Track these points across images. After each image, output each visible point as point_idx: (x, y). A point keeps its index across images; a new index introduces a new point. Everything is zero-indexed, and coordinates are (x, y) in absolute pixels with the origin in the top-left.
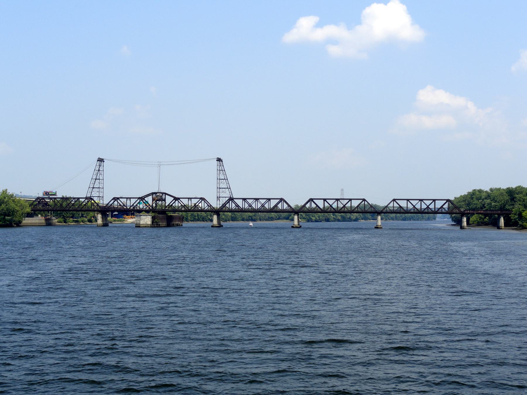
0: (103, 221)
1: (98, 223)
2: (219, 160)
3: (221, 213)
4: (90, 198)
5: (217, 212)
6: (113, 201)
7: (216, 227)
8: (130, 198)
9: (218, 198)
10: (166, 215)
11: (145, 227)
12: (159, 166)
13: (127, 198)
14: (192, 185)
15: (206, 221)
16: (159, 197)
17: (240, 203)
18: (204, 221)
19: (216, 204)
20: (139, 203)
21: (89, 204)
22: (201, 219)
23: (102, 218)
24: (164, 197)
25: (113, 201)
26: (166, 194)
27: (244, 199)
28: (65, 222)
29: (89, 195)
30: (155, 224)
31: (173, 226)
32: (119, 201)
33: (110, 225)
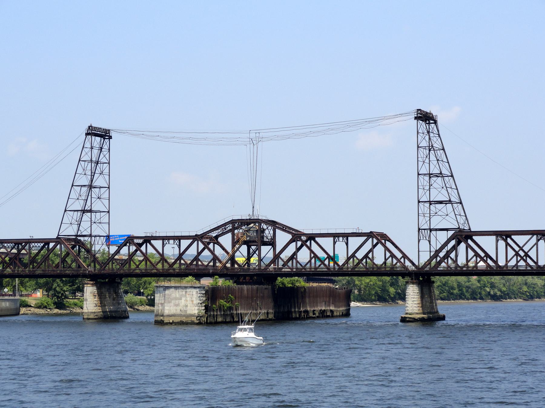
0: (102, 304)
1: (85, 310)
2: (425, 117)
3: (438, 280)
4: (76, 242)
5: (423, 277)
6: (453, 243)
7: (414, 320)
8: (346, 236)
9: (425, 232)
10: (273, 287)
11: (181, 323)
12: (255, 140)
13: (335, 236)
14: (346, 194)
15: (481, 298)
16: (252, 231)
17: (488, 243)
18: (475, 299)
19: (418, 253)
20: (454, 248)
21: (139, 257)
22: (468, 295)
23: (101, 296)
24: (268, 233)
25: (453, 243)
26: (274, 224)
27: (504, 235)
28: (60, 305)
29: (70, 231)
30: (218, 314)
31: (305, 317)
32: (314, 247)
33: (133, 317)
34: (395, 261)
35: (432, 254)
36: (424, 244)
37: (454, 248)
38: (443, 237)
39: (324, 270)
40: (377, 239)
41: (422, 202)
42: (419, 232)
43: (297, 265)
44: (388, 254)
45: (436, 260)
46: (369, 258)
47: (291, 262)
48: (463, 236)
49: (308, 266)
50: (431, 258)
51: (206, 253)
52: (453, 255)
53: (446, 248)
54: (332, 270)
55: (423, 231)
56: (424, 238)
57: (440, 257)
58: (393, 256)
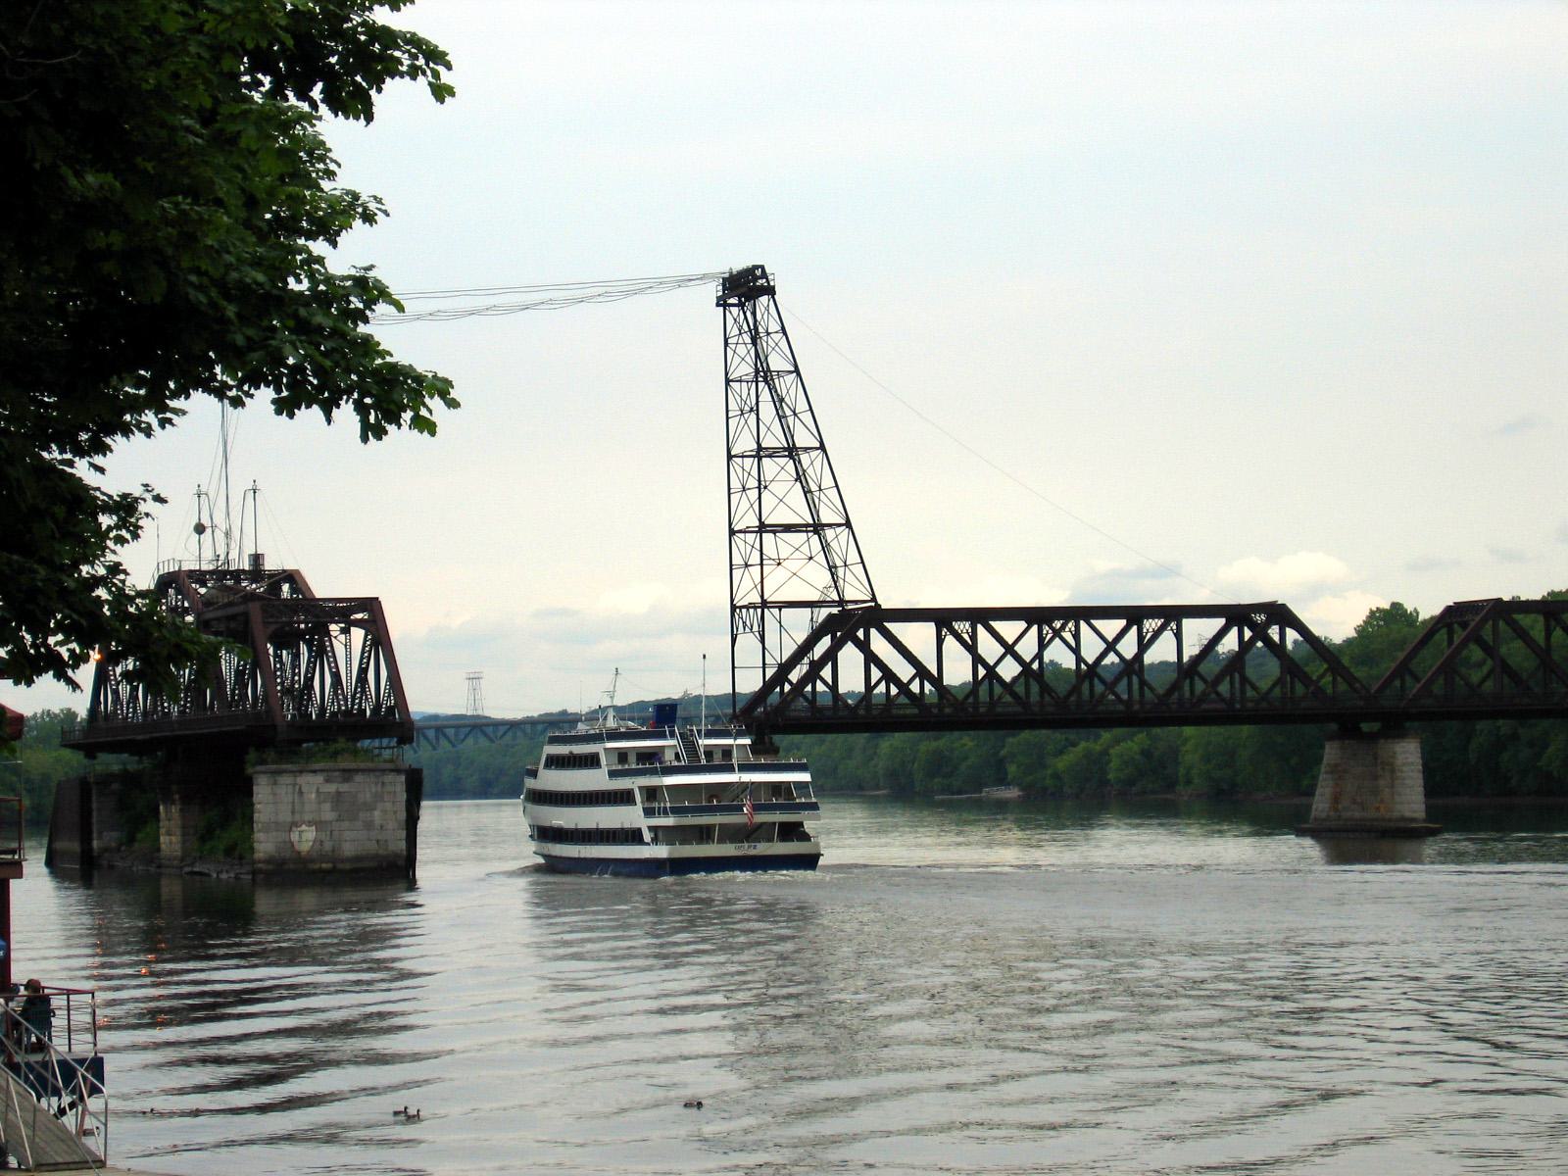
6: (825, 642)
25: (825, 642)
32: (879, 645)
34: (894, 690)
35: (770, 672)
36: (748, 642)
37: (831, 656)
38: (799, 625)
39: (908, 711)
40: (1253, 626)
41: (740, 531)
42: (733, 616)
43: (1142, 694)
44: (876, 674)
45: (782, 689)
46: (825, 682)
47: (1124, 682)
48: (853, 622)
49: (1277, 691)
50: (768, 686)
51: (1476, 653)
52: (826, 673)
53: (810, 655)
54: (1036, 709)
55: (744, 611)
56: (747, 630)
57: (790, 683)
58: (889, 676)
